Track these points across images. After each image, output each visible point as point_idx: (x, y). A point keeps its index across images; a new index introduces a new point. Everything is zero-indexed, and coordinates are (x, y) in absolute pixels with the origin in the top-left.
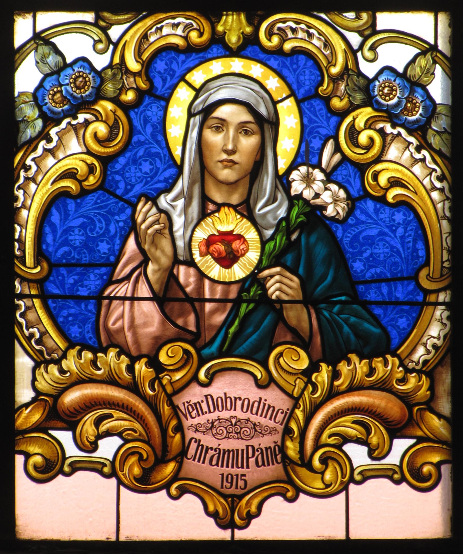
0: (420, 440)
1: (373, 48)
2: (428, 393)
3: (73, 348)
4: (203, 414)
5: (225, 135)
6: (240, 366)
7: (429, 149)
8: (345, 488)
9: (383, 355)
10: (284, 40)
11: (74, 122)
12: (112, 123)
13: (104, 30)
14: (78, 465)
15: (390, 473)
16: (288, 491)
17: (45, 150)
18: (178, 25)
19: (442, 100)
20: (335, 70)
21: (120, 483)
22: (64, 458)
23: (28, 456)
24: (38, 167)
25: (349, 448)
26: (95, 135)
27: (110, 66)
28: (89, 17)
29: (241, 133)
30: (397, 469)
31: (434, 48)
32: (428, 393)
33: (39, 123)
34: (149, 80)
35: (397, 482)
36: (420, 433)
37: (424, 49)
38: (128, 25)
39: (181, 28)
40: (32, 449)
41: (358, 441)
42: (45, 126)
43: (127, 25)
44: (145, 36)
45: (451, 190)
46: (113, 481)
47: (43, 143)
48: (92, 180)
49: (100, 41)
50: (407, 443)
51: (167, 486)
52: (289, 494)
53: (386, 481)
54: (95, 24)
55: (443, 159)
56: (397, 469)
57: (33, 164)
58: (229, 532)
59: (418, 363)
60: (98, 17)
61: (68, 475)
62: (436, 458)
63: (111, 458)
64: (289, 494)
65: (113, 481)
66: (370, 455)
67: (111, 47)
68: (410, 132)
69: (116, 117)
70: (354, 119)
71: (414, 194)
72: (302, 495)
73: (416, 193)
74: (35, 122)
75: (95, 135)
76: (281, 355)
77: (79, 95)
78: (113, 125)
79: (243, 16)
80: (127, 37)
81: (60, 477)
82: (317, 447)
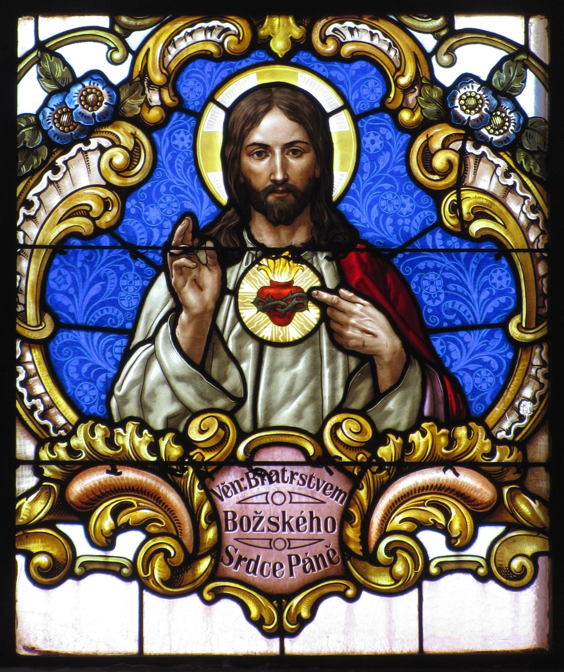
0: (510, 527)
1: (451, 51)
2: (520, 452)
3: (85, 422)
4: (241, 490)
5: (270, 161)
6: (288, 439)
7: (519, 172)
8: (418, 585)
9: (464, 422)
10: (340, 44)
11: (85, 148)
12: (132, 148)
13: (122, 38)
14: (91, 567)
15: (474, 567)
16: (348, 588)
17: (50, 182)
18: (211, 29)
19: (537, 111)
20: (403, 81)
21: (143, 587)
22: (75, 558)
23: (29, 556)
24: (41, 202)
25: (424, 536)
26: (111, 161)
27: (128, 81)
28: (104, 21)
29: (287, 154)
30: (483, 562)
31: (525, 49)
32: (520, 452)
33: (45, 151)
34: (176, 93)
35: (483, 579)
36: (510, 519)
37: (511, 52)
38: (148, 31)
39: (216, 32)
40: (34, 547)
41: (435, 527)
42: (50, 154)
43: (148, 31)
44: (170, 42)
45: (545, 222)
46: (135, 585)
47: (49, 173)
48: (108, 218)
49: (116, 49)
50: (496, 531)
51: (199, 591)
52: (350, 592)
53: (469, 578)
54: (110, 30)
55: (536, 184)
56: (483, 562)
57: (35, 199)
58: (276, 642)
59: (508, 432)
60: (113, 22)
61: (78, 578)
62: (530, 549)
63: (131, 558)
64: (350, 592)
65: (135, 585)
66: (450, 545)
67: (130, 57)
68: (496, 151)
69: (137, 140)
70: (429, 139)
71: (503, 228)
72: (364, 594)
73: (505, 226)
74: (38, 149)
75: (111, 161)
76: (338, 425)
77: (91, 113)
78: (133, 150)
79: (291, 20)
80: (150, 44)
81: (70, 583)
82: (383, 534)
